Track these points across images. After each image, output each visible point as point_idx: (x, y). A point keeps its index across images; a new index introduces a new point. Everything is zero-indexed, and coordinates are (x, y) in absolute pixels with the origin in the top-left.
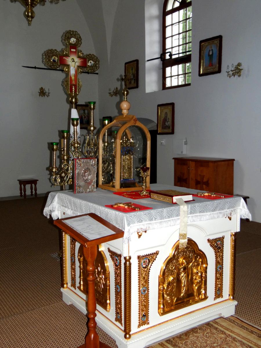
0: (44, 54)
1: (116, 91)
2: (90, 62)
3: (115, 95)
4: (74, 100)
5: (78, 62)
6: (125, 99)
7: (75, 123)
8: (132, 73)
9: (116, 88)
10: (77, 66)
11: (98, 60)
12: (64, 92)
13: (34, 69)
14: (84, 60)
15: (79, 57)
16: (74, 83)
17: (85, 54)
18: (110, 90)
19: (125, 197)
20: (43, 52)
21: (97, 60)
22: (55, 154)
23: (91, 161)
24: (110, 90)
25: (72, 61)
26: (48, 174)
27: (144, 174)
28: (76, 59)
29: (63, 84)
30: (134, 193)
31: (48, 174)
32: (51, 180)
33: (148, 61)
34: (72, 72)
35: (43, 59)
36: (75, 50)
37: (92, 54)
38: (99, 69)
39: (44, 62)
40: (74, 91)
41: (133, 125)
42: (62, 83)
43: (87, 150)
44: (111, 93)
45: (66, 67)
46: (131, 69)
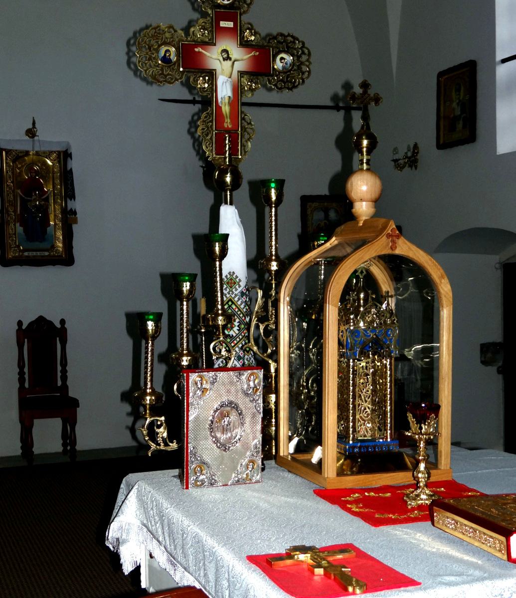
0: (132, 42)
1: (414, 152)
2: (282, 59)
3: (410, 166)
4: (228, 179)
5: (241, 58)
6: (365, 165)
7: (217, 249)
8: (457, 101)
9: (412, 146)
10: (238, 72)
11: (306, 51)
12: (198, 153)
13: (192, 105)
14: (262, 52)
15: (244, 44)
16: (228, 124)
17: (263, 34)
18: (395, 150)
19: (349, 511)
20: (131, 34)
21: (303, 53)
22: (152, 349)
23: (244, 377)
24: (395, 150)
25: (221, 59)
26: (129, 414)
27: (421, 428)
28: (236, 52)
29: (193, 130)
30: (388, 495)
31: (129, 414)
32: (138, 433)
33: (504, 61)
34: (224, 91)
35: (131, 54)
36: (230, 24)
37: (286, 34)
38: (311, 77)
39: (132, 66)
40: (229, 148)
41: (387, 251)
42: (191, 127)
43: (256, 335)
44: (400, 159)
45: (204, 79)
46: (454, 91)
